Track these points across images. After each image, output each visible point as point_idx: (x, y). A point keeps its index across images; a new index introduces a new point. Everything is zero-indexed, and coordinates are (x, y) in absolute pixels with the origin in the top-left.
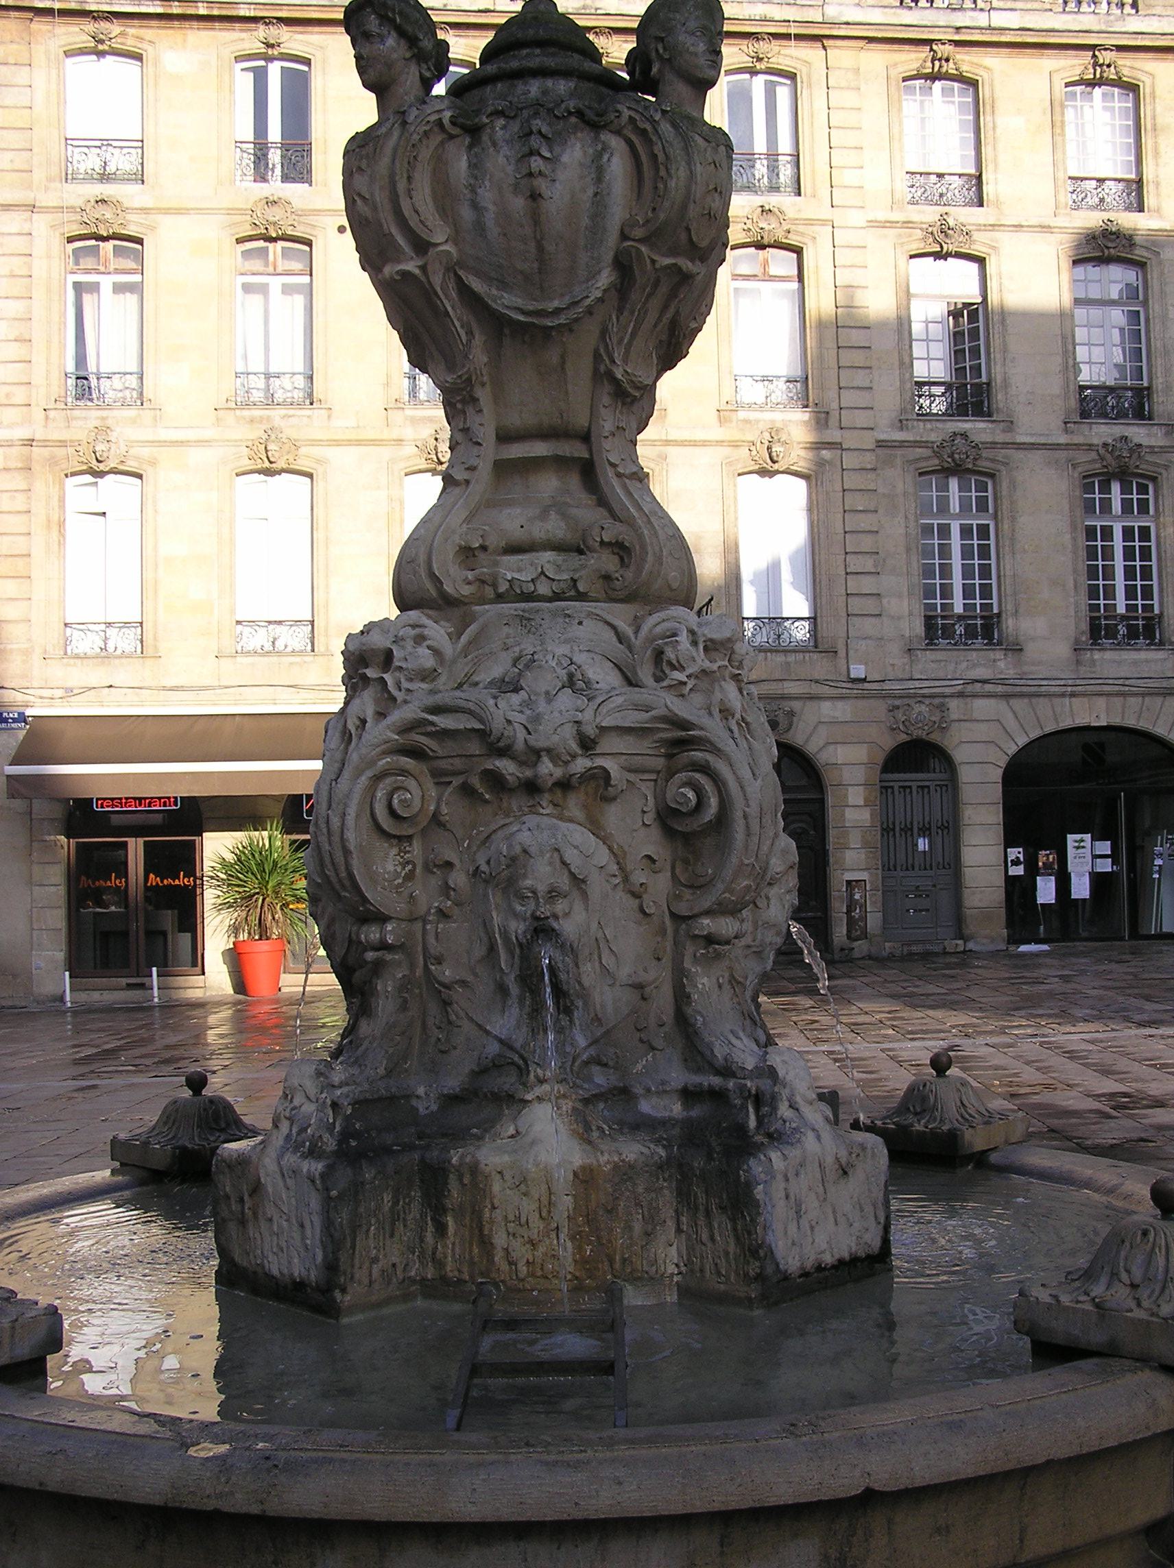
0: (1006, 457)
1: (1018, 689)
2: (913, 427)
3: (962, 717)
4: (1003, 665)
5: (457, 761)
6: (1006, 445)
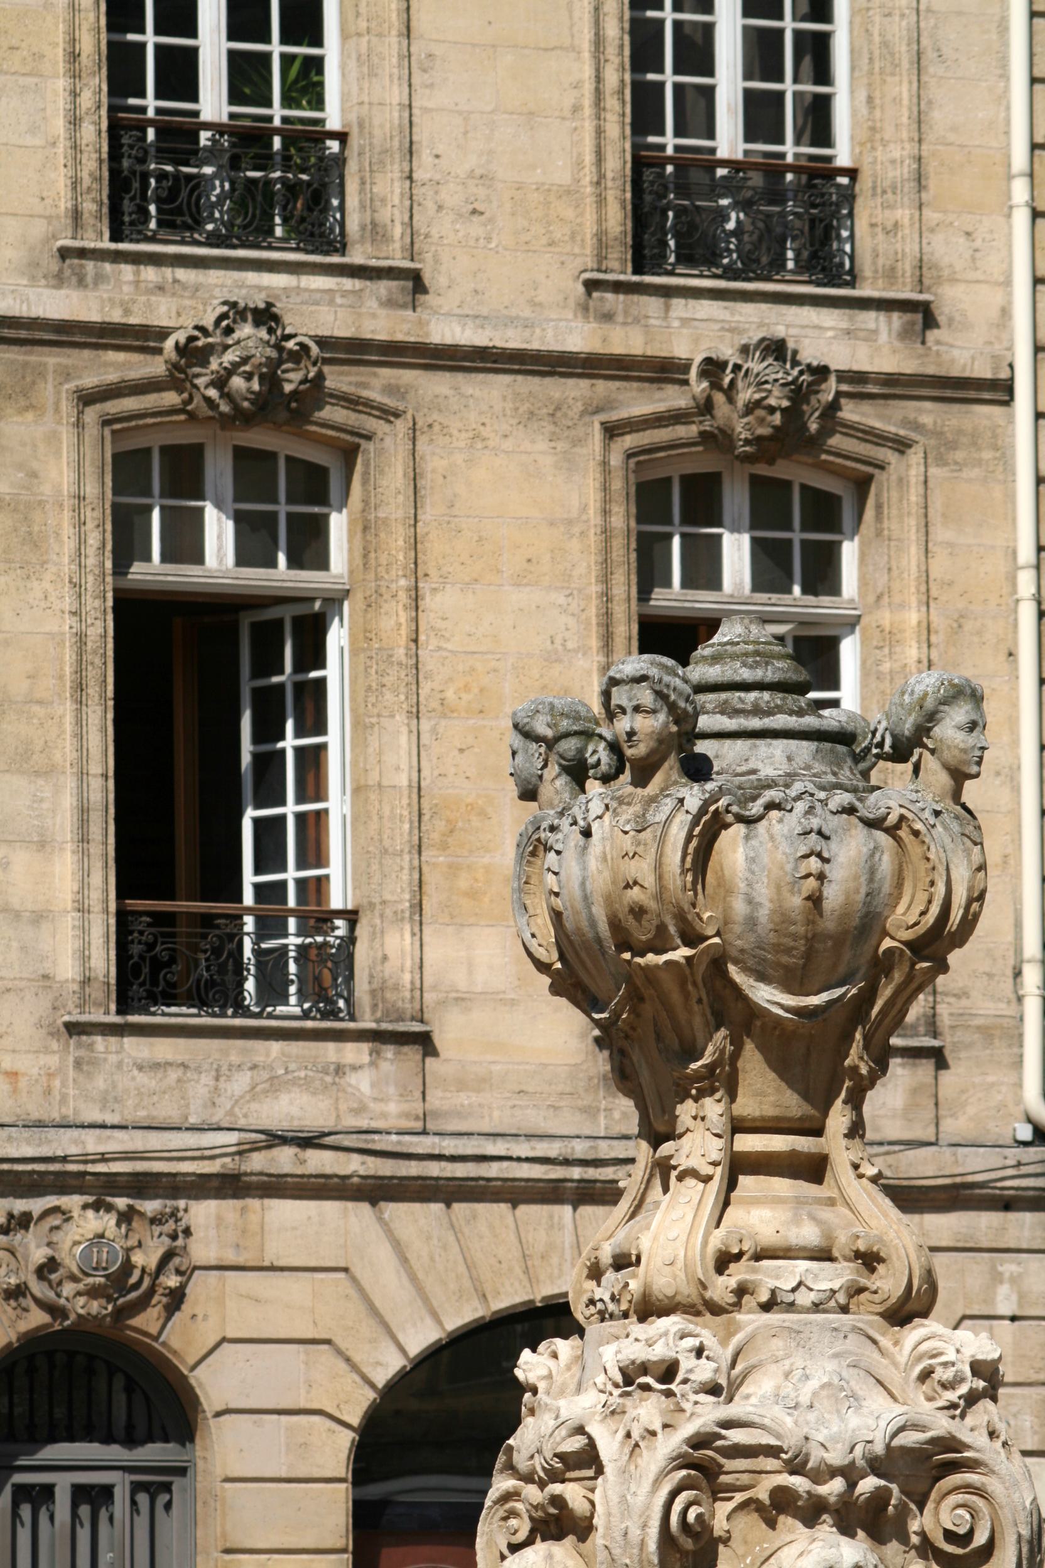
0: (391, 389)
1: (413, 1169)
2: (99, 278)
3: (231, 1258)
4: (364, 1090)
5: (745, 1476)
6: (395, 353)
